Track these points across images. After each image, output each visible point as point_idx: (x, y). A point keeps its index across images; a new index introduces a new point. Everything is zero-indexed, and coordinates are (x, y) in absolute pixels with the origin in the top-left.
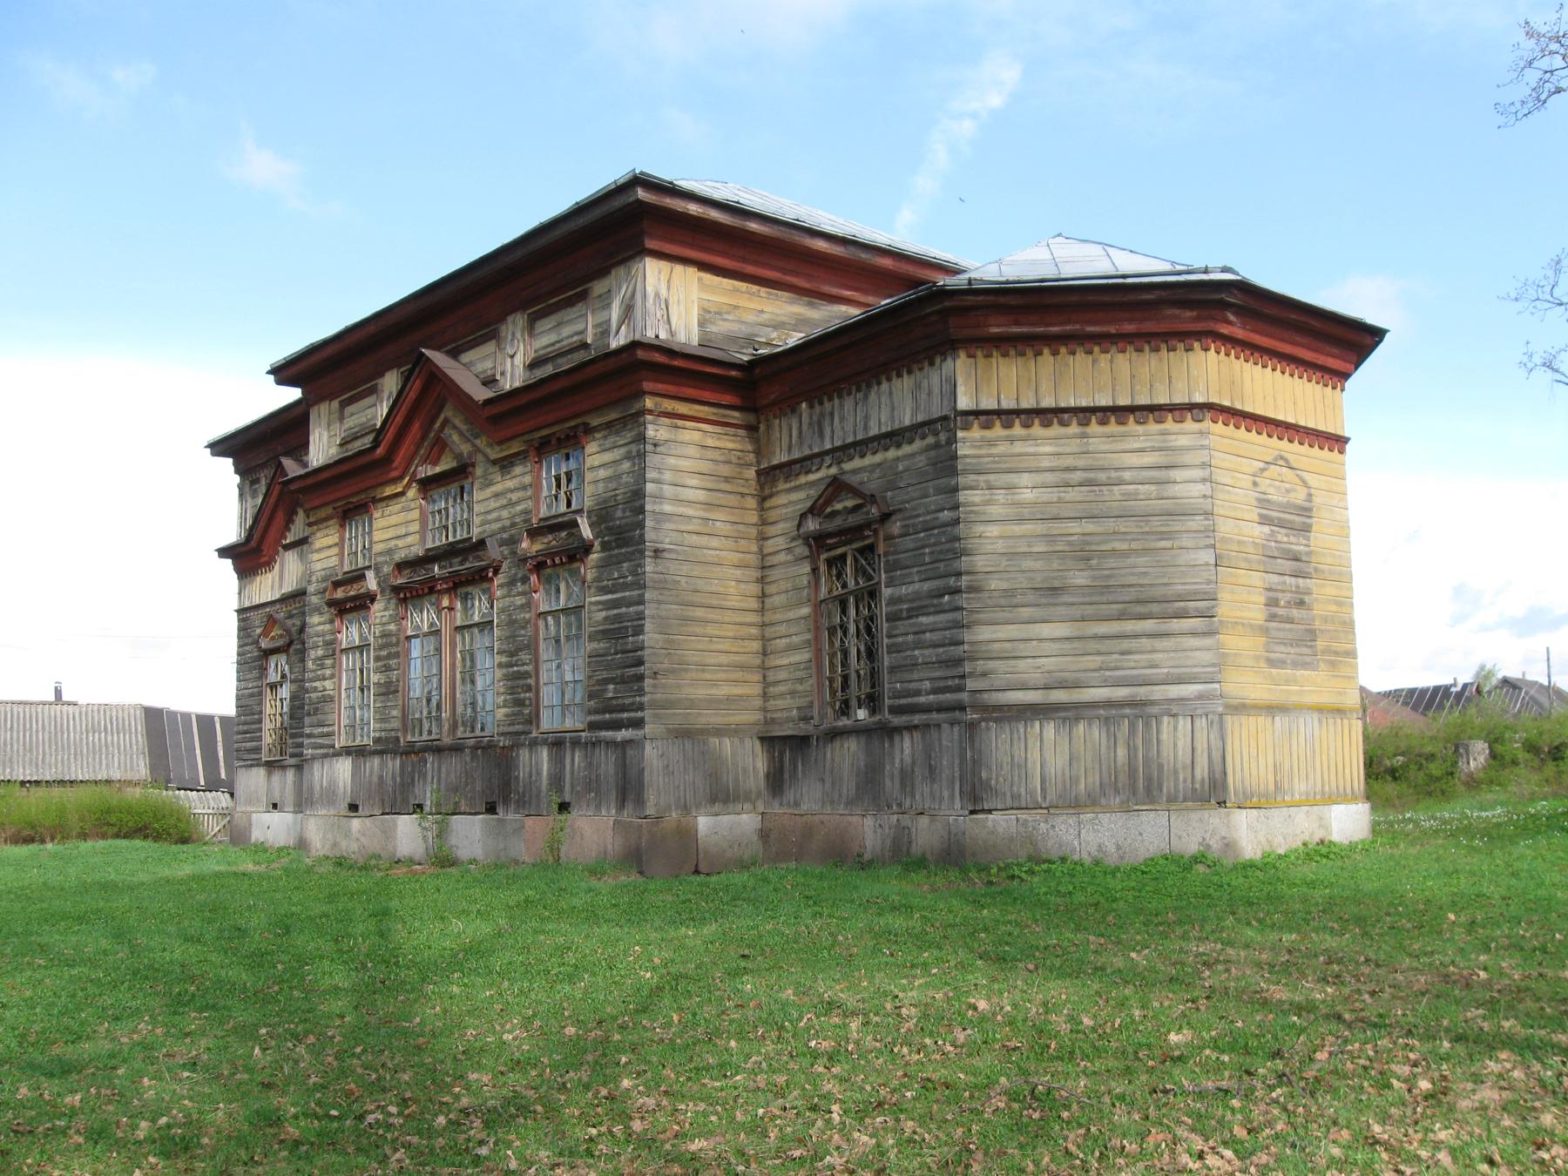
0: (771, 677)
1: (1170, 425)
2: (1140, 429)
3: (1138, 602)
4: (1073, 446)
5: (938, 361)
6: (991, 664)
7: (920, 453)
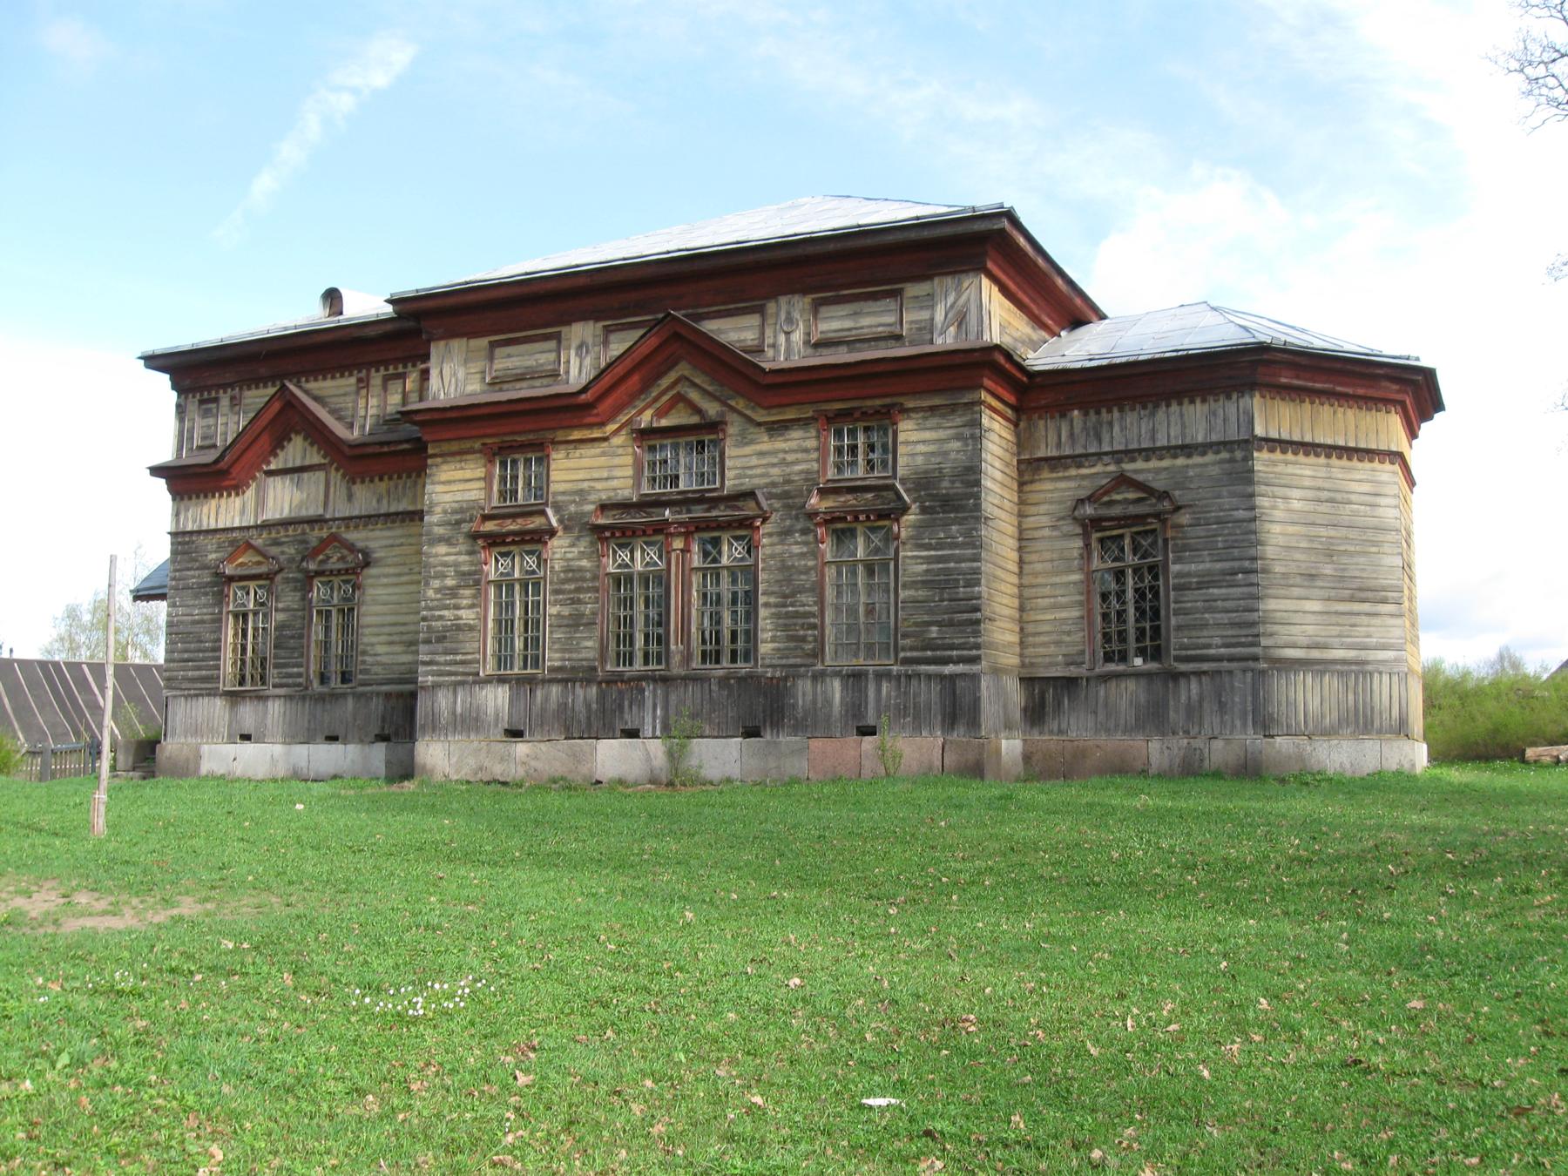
0: (1030, 628)
1: (1376, 465)
2: (1360, 465)
3: (1360, 589)
4: (1322, 473)
5: (1235, 396)
6: (1276, 628)
7: (1214, 464)
